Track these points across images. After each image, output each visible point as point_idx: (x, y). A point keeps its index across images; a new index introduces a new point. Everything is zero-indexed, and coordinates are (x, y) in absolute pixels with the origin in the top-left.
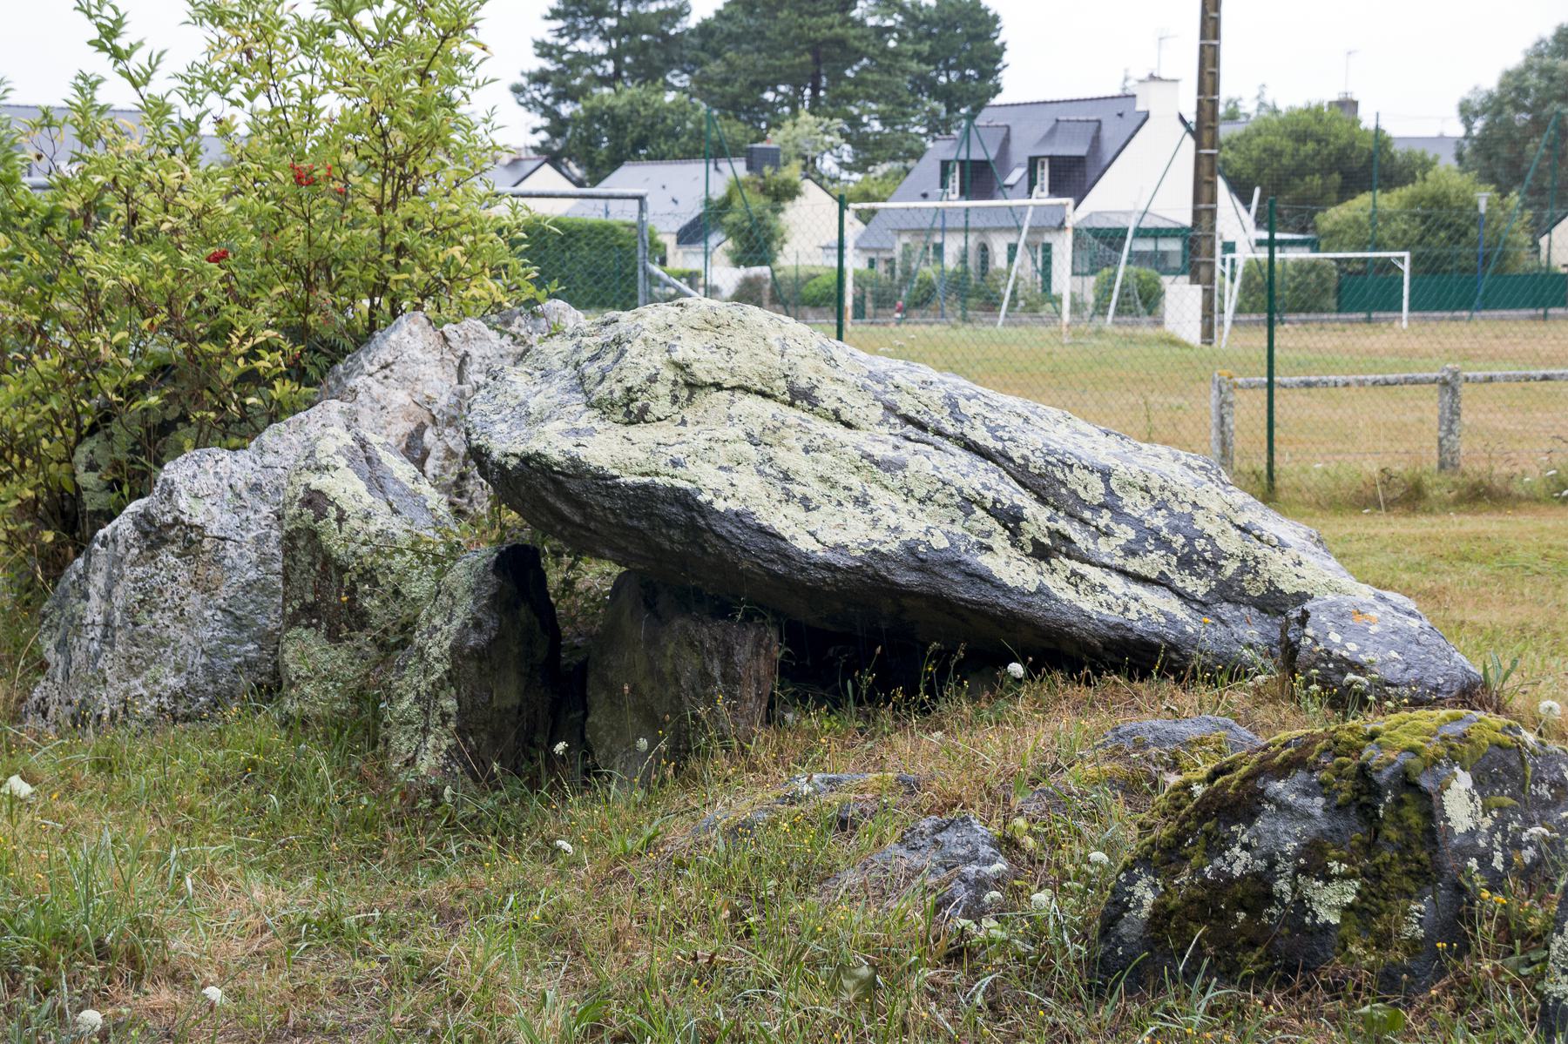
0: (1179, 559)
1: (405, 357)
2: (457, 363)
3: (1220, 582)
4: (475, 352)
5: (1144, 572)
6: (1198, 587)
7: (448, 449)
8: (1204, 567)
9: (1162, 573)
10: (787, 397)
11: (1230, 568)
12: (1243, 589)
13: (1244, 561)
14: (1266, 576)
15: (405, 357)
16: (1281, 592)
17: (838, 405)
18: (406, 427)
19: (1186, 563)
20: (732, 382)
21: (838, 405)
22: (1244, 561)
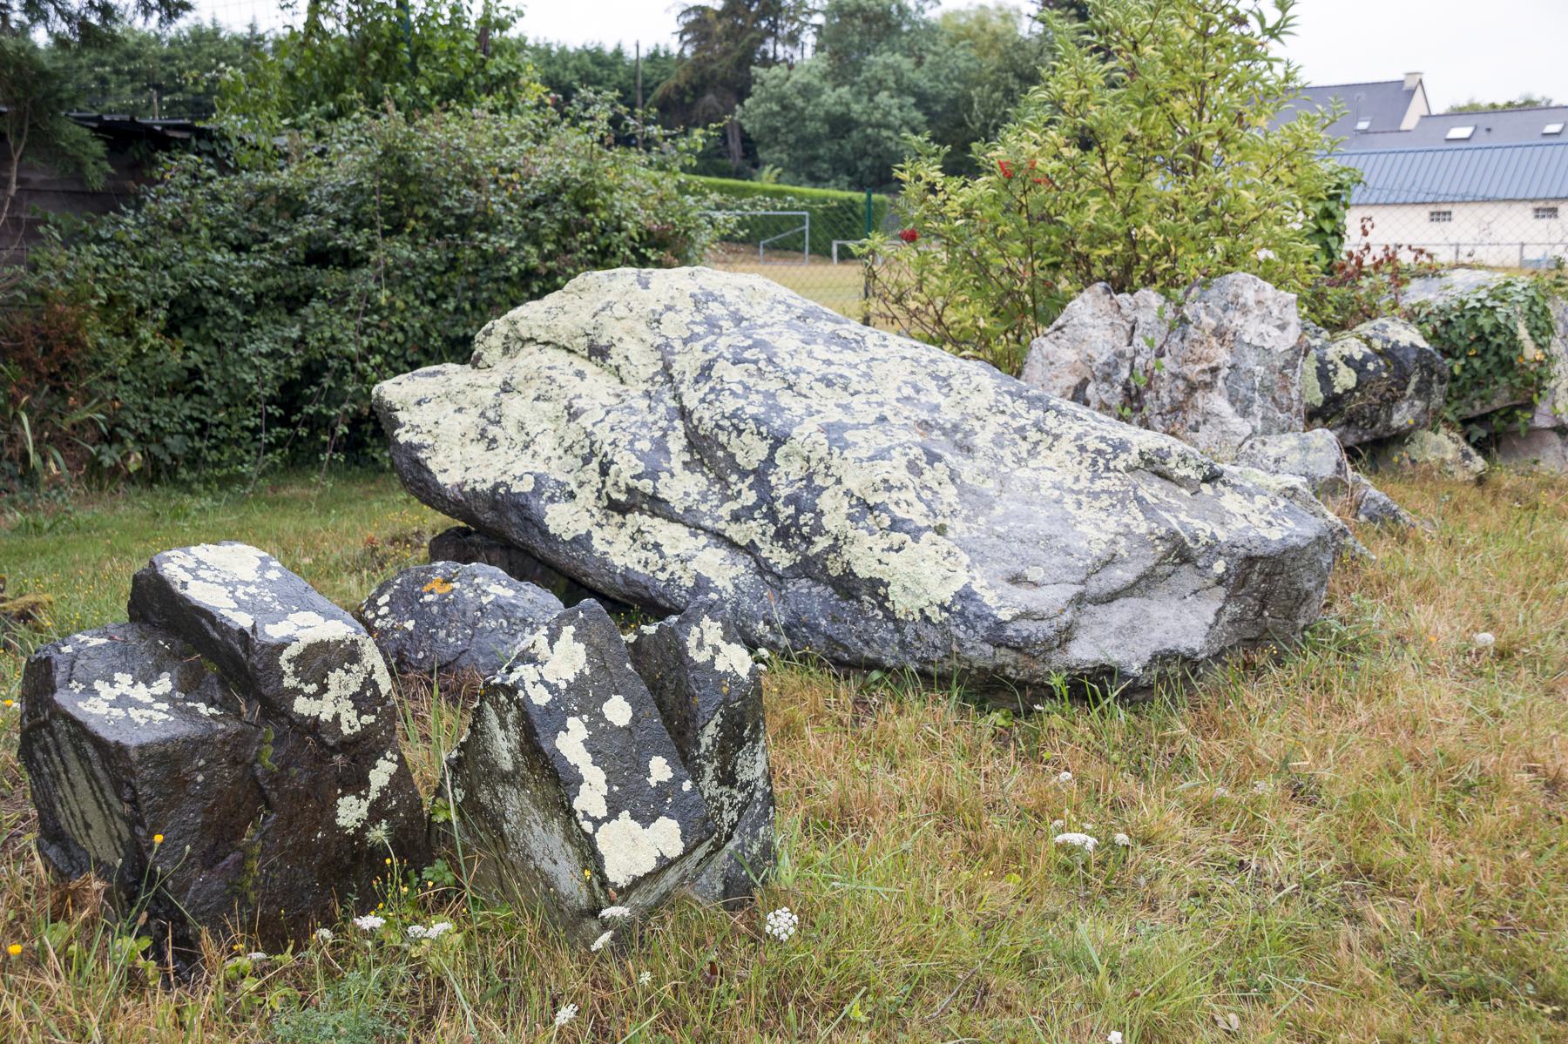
0: (777, 531)
1: (1075, 321)
2: (1128, 327)
3: (806, 559)
4: (1141, 319)
5: (736, 538)
6: (781, 558)
7: (1102, 402)
8: (797, 541)
9: (752, 541)
10: (586, 354)
11: (822, 543)
12: (825, 567)
13: (836, 539)
14: (846, 557)
15: (1075, 321)
16: (855, 575)
17: (622, 362)
18: (1074, 380)
19: (782, 535)
20: (544, 337)
21: (622, 362)
22: (836, 539)
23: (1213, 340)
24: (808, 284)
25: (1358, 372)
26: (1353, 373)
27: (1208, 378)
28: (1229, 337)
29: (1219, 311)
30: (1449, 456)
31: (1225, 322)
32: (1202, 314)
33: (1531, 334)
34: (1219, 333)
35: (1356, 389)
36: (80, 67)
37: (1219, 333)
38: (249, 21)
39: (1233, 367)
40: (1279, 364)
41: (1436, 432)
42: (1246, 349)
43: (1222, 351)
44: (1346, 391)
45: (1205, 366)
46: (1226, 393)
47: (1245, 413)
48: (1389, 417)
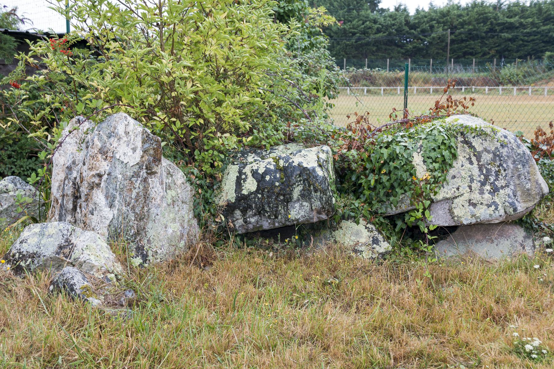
23: (99, 156)
24: (340, 113)
25: (258, 182)
26: (256, 183)
27: (97, 180)
28: (110, 154)
29: (105, 138)
30: (363, 240)
31: (108, 145)
32: (96, 139)
33: (424, 162)
34: (103, 152)
35: (257, 191)
36: (424, 22)
37: (103, 152)
38: (429, 2)
39: (109, 174)
40: (129, 174)
41: (358, 223)
42: (117, 163)
43: (105, 163)
44: (251, 193)
45: (94, 172)
46: (104, 191)
47: (111, 206)
48: (287, 212)
